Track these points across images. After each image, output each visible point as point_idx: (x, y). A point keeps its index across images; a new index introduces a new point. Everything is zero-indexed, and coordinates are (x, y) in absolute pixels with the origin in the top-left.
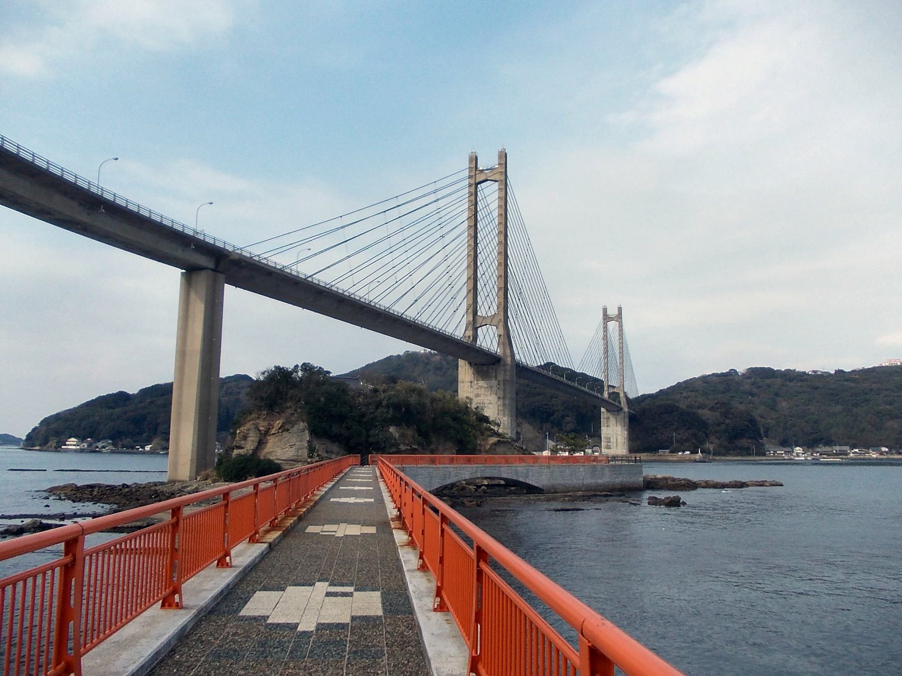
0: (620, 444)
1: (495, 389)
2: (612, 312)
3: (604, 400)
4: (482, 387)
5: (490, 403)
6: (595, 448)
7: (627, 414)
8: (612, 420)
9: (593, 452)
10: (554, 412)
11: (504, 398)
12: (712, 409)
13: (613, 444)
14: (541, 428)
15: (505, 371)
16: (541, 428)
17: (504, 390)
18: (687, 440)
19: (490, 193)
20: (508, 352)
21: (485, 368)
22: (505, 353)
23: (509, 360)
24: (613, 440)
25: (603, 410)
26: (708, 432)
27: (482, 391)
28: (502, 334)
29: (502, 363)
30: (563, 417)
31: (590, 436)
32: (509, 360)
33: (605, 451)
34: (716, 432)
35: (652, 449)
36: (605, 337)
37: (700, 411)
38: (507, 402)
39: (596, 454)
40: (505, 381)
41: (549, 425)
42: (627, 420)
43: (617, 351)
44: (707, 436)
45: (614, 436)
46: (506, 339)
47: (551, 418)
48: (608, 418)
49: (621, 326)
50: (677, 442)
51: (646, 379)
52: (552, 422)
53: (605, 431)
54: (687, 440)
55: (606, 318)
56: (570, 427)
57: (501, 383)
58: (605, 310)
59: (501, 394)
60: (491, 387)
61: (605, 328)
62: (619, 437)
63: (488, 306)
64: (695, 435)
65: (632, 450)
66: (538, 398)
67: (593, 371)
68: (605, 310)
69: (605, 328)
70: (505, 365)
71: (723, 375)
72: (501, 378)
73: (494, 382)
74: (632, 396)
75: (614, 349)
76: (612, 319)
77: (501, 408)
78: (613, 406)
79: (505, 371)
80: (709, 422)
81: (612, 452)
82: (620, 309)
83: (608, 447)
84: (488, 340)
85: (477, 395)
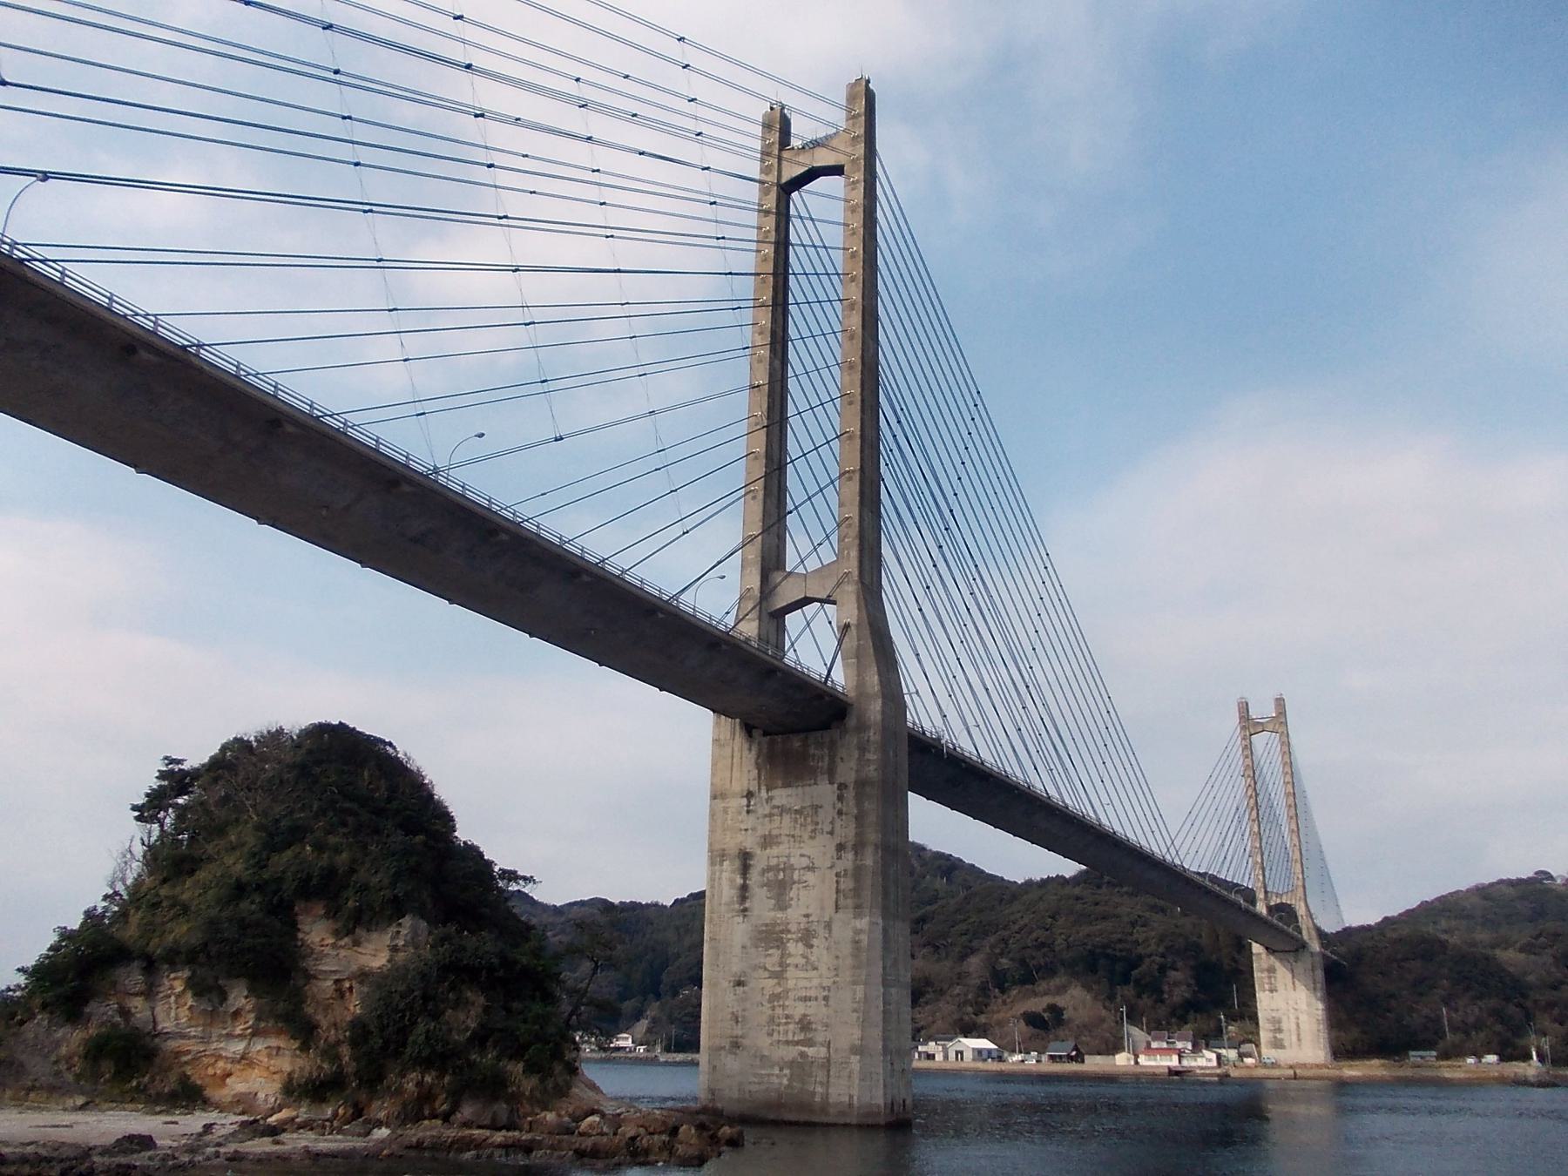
0: (1307, 1037)
1: (827, 814)
2: (1262, 710)
3: (1257, 917)
4: (783, 810)
5: (811, 868)
6: (1246, 1048)
7: (1318, 959)
8: (1283, 973)
9: (1241, 1056)
10: (1140, 958)
11: (859, 847)
12: (1527, 949)
13: (1289, 1037)
14: (1111, 998)
15: (863, 749)
16: (1111, 998)
17: (859, 818)
18: (1478, 1026)
19: (824, 208)
20: (873, 680)
21: (796, 743)
22: (860, 684)
23: (875, 709)
24: (1288, 1025)
25: (1257, 948)
26: (1529, 1004)
27: (785, 825)
28: (853, 620)
29: (852, 722)
30: (1163, 969)
31: (1232, 1018)
32: (875, 709)
33: (1268, 1053)
34: (1551, 1005)
35: (1389, 1047)
36: (1252, 772)
37: (1499, 954)
38: (869, 859)
39: (1249, 1061)
40: (861, 784)
41: (1129, 991)
42: (1320, 974)
43: (1282, 811)
44: (1529, 1017)
45: (1291, 1018)
46: (874, 640)
47: (1135, 973)
48: (1271, 970)
49: (1286, 744)
50: (1454, 1029)
51: (1363, 893)
52: (1137, 982)
53: (1265, 1002)
54: (1478, 1026)
55: (1249, 725)
56: (1180, 994)
57: (850, 794)
58: (1244, 708)
59: (846, 830)
60: (816, 808)
61: (1248, 748)
62: (1303, 1018)
63: (813, 545)
64: (1498, 1015)
65: (1340, 1052)
66: (1101, 926)
67: (1238, 871)
68: (1244, 708)
69: (1248, 748)
70: (862, 727)
71: (1520, 881)
72: (847, 771)
73: (824, 791)
74: (1330, 927)
75: (1270, 798)
76: (1259, 727)
77: (847, 884)
78: (1281, 928)
79: (863, 749)
80: (1531, 978)
81: (1286, 1056)
82: (1280, 703)
83: (1278, 1044)
84: (815, 647)
85: (768, 841)
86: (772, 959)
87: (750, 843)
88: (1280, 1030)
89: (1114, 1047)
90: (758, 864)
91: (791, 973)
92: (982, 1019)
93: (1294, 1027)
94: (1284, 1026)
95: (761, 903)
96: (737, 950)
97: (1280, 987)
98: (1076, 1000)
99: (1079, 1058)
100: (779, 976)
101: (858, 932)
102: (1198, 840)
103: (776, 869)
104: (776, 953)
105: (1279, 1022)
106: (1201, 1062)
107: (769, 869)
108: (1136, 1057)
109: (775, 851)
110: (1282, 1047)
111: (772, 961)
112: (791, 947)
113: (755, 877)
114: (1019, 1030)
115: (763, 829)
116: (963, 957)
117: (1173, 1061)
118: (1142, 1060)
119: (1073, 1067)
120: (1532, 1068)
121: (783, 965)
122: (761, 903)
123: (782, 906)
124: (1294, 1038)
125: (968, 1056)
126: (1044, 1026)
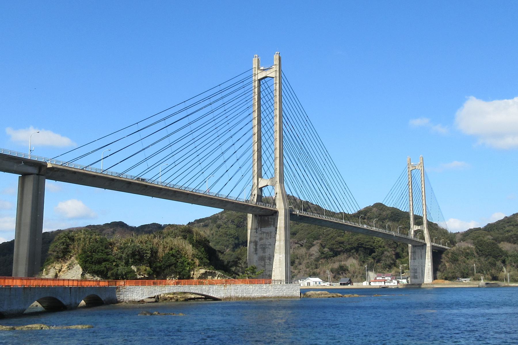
85: (261, 239)
86: (263, 263)
87: (257, 239)
88: (416, 272)
89: (364, 278)
90: (259, 243)
91: (267, 266)
92: (318, 271)
93: (420, 271)
94: (418, 271)
95: (260, 251)
96: (255, 261)
97: (417, 258)
98: (352, 263)
99: (350, 282)
100: (264, 266)
101: (280, 258)
102: (392, 200)
103: (263, 245)
104: (263, 262)
105: (416, 269)
106: (392, 284)
107: (261, 245)
108: (370, 283)
109: (262, 241)
110: (417, 278)
111: (263, 263)
112: (266, 261)
113: (258, 247)
114: (330, 275)
115: (260, 236)
116: (309, 248)
117: (382, 284)
118: (372, 284)
119: (349, 286)
120: (482, 282)
121: (265, 264)
122: (260, 251)
123: (264, 252)
124: (421, 275)
125: (312, 284)
126: (340, 272)
